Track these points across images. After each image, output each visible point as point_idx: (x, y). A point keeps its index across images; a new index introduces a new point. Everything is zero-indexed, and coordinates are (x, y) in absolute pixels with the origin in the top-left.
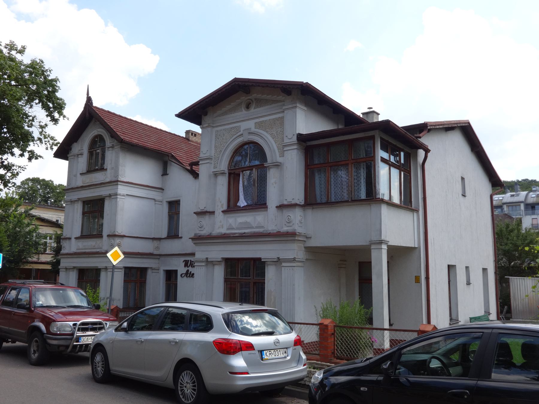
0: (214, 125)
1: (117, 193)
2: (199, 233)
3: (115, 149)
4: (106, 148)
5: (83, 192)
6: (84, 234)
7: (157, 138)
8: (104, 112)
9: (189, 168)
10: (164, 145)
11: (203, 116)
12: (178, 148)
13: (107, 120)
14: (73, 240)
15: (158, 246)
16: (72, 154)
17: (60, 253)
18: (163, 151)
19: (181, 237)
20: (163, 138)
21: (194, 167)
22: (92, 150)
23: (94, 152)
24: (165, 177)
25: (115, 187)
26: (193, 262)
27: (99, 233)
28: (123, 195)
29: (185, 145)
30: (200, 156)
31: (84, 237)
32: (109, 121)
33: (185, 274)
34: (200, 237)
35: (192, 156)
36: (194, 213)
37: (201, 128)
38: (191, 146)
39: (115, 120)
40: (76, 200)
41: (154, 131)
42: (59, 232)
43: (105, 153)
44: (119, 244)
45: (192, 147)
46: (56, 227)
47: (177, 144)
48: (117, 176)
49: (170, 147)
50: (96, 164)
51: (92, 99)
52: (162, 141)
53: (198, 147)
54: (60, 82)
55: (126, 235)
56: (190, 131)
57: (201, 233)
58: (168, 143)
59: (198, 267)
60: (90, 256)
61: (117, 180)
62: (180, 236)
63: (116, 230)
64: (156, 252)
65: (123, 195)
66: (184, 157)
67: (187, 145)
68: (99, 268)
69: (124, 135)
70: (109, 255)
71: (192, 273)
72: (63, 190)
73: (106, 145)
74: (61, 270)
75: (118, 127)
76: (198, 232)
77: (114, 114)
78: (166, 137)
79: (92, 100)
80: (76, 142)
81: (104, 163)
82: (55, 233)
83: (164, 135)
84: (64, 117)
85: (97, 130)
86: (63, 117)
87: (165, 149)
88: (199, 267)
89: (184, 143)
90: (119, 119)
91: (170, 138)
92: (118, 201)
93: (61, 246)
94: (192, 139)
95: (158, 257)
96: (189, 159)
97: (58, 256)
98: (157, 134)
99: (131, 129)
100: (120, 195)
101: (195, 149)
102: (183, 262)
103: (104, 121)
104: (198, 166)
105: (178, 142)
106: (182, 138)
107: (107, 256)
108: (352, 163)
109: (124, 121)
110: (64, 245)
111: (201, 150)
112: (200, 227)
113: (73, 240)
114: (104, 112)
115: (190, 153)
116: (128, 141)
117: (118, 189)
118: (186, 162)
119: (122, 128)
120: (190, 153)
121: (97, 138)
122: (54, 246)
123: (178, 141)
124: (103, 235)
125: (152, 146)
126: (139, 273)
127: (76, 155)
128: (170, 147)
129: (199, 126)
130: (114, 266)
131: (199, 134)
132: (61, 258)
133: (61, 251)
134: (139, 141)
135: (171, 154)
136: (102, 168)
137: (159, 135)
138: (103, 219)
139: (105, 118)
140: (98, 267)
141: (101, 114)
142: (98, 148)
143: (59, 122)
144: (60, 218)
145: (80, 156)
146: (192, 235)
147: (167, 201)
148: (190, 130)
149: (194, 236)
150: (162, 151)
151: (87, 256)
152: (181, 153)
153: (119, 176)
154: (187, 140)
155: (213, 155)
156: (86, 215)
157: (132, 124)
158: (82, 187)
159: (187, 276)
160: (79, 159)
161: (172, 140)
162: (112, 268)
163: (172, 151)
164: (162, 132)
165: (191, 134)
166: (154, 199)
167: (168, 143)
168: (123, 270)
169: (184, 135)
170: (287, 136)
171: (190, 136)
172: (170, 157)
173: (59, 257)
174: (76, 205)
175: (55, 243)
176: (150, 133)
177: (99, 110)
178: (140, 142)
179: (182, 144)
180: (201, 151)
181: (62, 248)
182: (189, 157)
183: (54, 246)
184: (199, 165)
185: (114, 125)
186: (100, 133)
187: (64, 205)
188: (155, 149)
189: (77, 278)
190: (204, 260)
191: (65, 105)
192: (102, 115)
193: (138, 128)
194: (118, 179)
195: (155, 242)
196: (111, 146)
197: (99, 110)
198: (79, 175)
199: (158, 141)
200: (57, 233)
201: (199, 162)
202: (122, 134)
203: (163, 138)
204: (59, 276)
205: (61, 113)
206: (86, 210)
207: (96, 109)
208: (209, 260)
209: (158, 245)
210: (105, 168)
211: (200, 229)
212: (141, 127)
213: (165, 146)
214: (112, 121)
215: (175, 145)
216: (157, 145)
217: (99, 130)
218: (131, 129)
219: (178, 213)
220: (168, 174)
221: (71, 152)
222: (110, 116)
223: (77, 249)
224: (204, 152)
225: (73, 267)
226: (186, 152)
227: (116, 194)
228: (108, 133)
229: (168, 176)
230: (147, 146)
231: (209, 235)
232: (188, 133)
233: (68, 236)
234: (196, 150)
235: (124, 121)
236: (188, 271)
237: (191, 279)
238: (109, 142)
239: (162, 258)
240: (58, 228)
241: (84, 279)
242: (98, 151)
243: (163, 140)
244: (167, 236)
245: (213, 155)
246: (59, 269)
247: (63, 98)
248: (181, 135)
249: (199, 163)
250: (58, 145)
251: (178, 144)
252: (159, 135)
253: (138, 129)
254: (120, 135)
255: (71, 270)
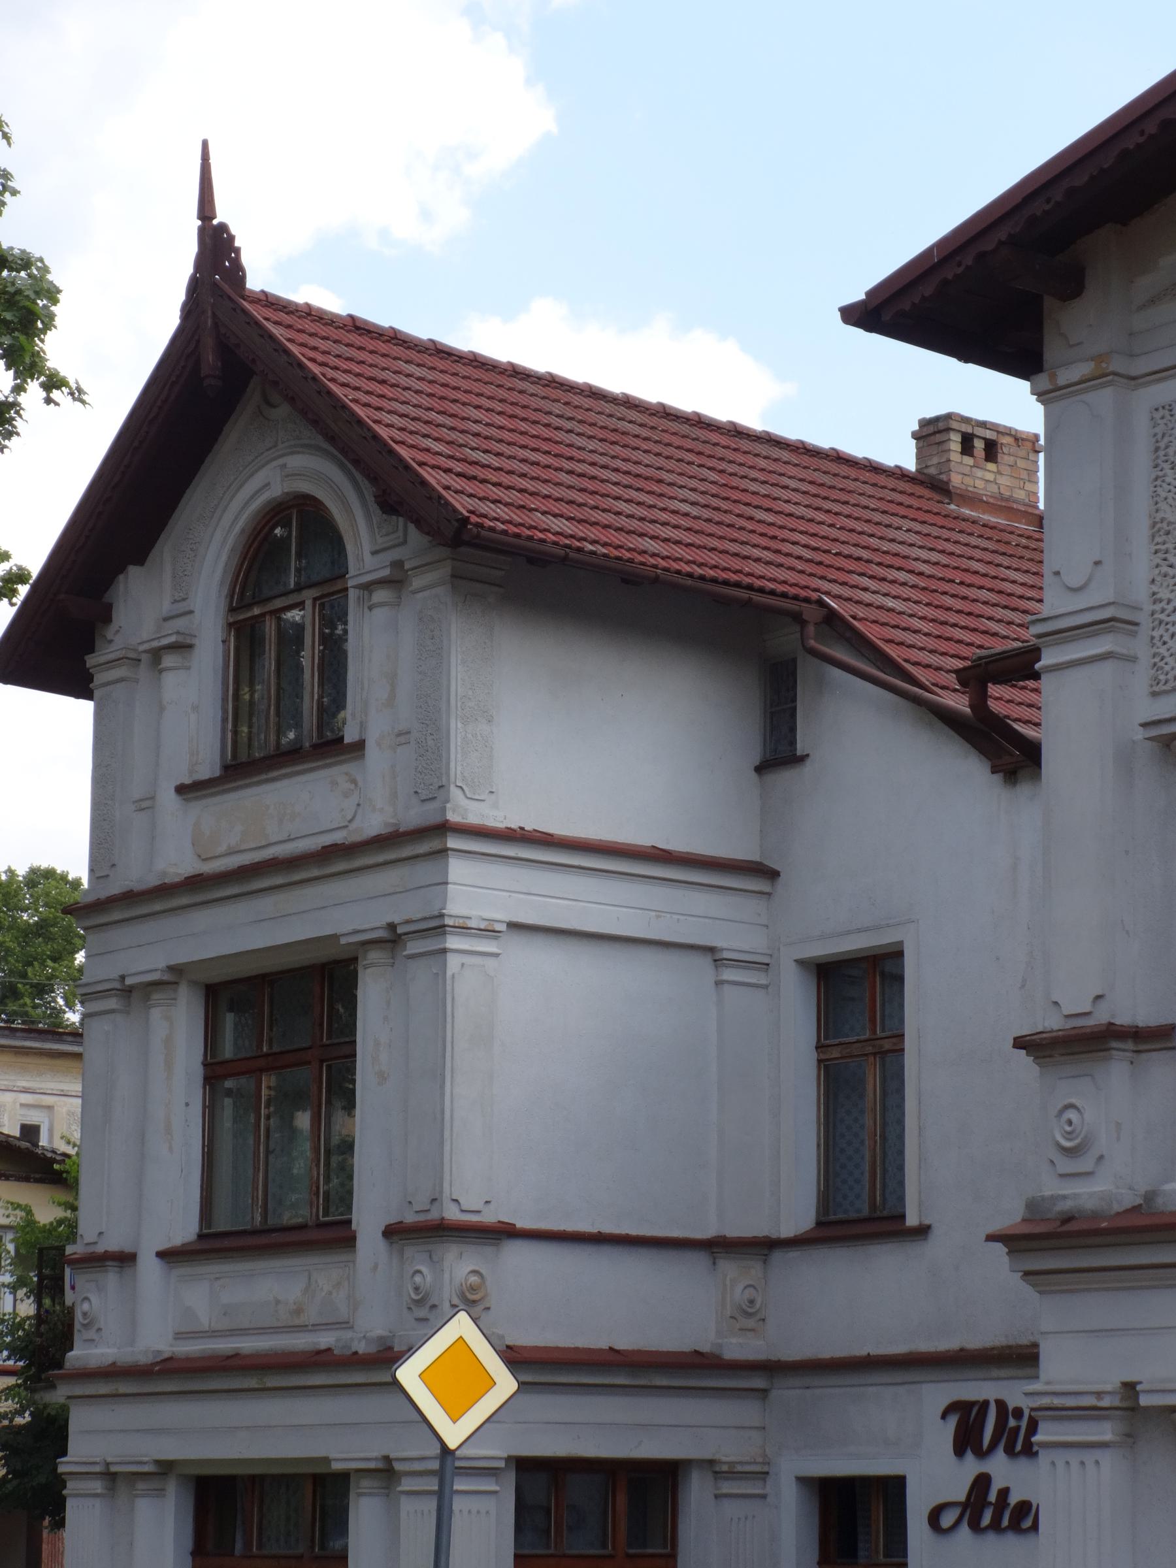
0: (1141, 366)
1: (442, 916)
2: (1064, 1197)
3: (414, 592)
4: (352, 594)
5: (202, 919)
6: (221, 1225)
7: (714, 489)
8: (324, 331)
9: (959, 703)
10: (763, 541)
11: (1048, 302)
12: (865, 554)
13: (344, 385)
14: (149, 1268)
15: (752, 1302)
16: (113, 647)
17: (60, 1365)
18: (761, 590)
19: (922, 1231)
20: (754, 487)
21: (1000, 697)
22: (256, 611)
23: (270, 628)
24: (785, 777)
25: (423, 872)
26: (1018, 1413)
27: (326, 1214)
28: (489, 932)
29: (917, 527)
30: (1046, 610)
31: (226, 1243)
32: (359, 395)
33: (965, 1506)
34: (1067, 1228)
35: (979, 608)
36: (1020, 1043)
37: (1041, 395)
38: (963, 538)
39: (403, 381)
40: (155, 977)
41: (688, 444)
42: (46, 1212)
43: (343, 617)
44: (472, 1289)
45: (974, 541)
46: (27, 1179)
47: (859, 526)
48: (438, 791)
49: (807, 554)
50: (288, 713)
51: (237, 244)
52: (750, 511)
53: (1014, 540)
54: (14, 138)
55: (522, 1223)
56: (954, 425)
57: (1076, 1196)
58: (791, 523)
59: (1060, 1457)
60: (273, 1381)
61: (437, 820)
62: (912, 1220)
63: (446, 1185)
64: (737, 1348)
65: (489, 932)
66: (916, 624)
67: (935, 531)
68: (336, 1466)
69: (469, 487)
70: (408, 1374)
71: (1013, 1499)
72: (69, 910)
73: (352, 571)
74: (71, 1486)
75: (426, 429)
76: (1050, 1187)
77: (395, 338)
78: (774, 478)
79: (237, 251)
80: (140, 560)
81: (339, 702)
82: (16, 1218)
83: (762, 463)
84: (53, 383)
85: (284, 466)
86: (43, 386)
87: (772, 572)
88: (1074, 1457)
89: (912, 513)
90: (431, 375)
91: (804, 487)
92: (449, 973)
93: (70, 1311)
94: (967, 480)
95: (758, 1382)
96: (958, 634)
97: (53, 1386)
98: (710, 463)
99: (523, 440)
100: (464, 930)
101: (999, 559)
102: (944, 1416)
103: (330, 393)
104: (1031, 684)
105: (867, 515)
106: (891, 483)
107: (396, 1384)
108: (322, 1061)
109: (464, 384)
110: (86, 1306)
111: (1050, 560)
112: (1067, 1151)
113: (149, 1268)
114: (324, 331)
115: (964, 591)
116: (505, 532)
117: (447, 883)
118: (934, 660)
119: (454, 436)
120: (964, 591)
121: (287, 525)
122: (15, 1314)
123: (864, 501)
124: (354, 1227)
125: (679, 551)
126: (622, 1500)
127: (144, 657)
128: (807, 554)
129: (1024, 386)
130: (445, 1451)
131: (1018, 438)
132: (69, 1397)
133: (71, 1349)
134: (580, 521)
135: (821, 603)
136: (329, 735)
137: (723, 466)
138: (354, 1106)
139: (331, 373)
140: (326, 1460)
141: (302, 345)
142: (292, 592)
143: (18, 423)
144: (50, 1108)
145: (168, 660)
146: (1010, 1216)
147: (802, 963)
148: (949, 416)
149: (1024, 1220)
150: (750, 587)
151: (252, 1383)
152: (895, 590)
153: (452, 788)
154: (927, 493)
155: (1140, 593)
156: (229, 1084)
157: (523, 399)
158: (195, 883)
159: (975, 1526)
160: (170, 680)
161: (819, 502)
162: (435, 1465)
163: (826, 586)
164: (745, 445)
165: (957, 447)
166: (711, 950)
167: (791, 523)
168: (511, 1479)
169: (904, 456)
170: (1057, 573)
171: (955, 456)
172: (811, 629)
173: (58, 1396)
174: (156, 1014)
175: (21, 1293)
176: (661, 462)
177: (288, 319)
178: (593, 532)
179: (897, 521)
180: (1047, 570)
181: (77, 1326)
182: (953, 618)
183: (15, 1314)
184: (1036, 676)
185: (395, 419)
186: (305, 487)
187: (73, 1017)
188: (702, 578)
189: (188, 1543)
190: (1106, 1402)
191: (55, 301)
192: (312, 354)
193: (568, 425)
194: (444, 810)
195: (729, 1268)
196: (386, 572)
197: (288, 319)
198: (168, 798)
199: (717, 516)
200: (30, 1222)
201: (1034, 653)
202: (458, 483)
203: (754, 487)
204: (60, 1524)
205: (27, 360)
206: (228, 1051)
207: (268, 313)
208: (1144, 1401)
209: (749, 1293)
210: (350, 735)
211: (1066, 1165)
212: (592, 417)
213: (774, 545)
214: (384, 390)
215: (843, 536)
216: (715, 543)
217: (297, 461)
218: (523, 440)
219: (887, 1044)
220: (802, 759)
221: (110, 633)
222: (370, 359)
223: (179, 1336)
224: (1075, 581)
225: (158, 1462)
226: (934, 585)
227: (437, 927)
228: (359, 477)
229: (808, 768)
230: (640, 558)
231: (1135, 1209)
232: (939, 438)
233: (112, 1244)
234: (1006, 561)
235: (464, 384)
236: (982, 1482)
237: (1009, 1546)
238: (367, 547)
239: (787, 1393)
240: (37, 1181)
241: (239, 1546)
242: (295, 615)
243: (756, 501)
244: (819, 1224)
245: (1140, 593)
246: (60, 1482)
247: (35, 251)
248: (889, 460)
249: (1037, 666)
250: (14, 592)
251: (867, 528)
252: (723, 466)
253: (573, 438)
254: (447, 488)
255: (141, 1486)
